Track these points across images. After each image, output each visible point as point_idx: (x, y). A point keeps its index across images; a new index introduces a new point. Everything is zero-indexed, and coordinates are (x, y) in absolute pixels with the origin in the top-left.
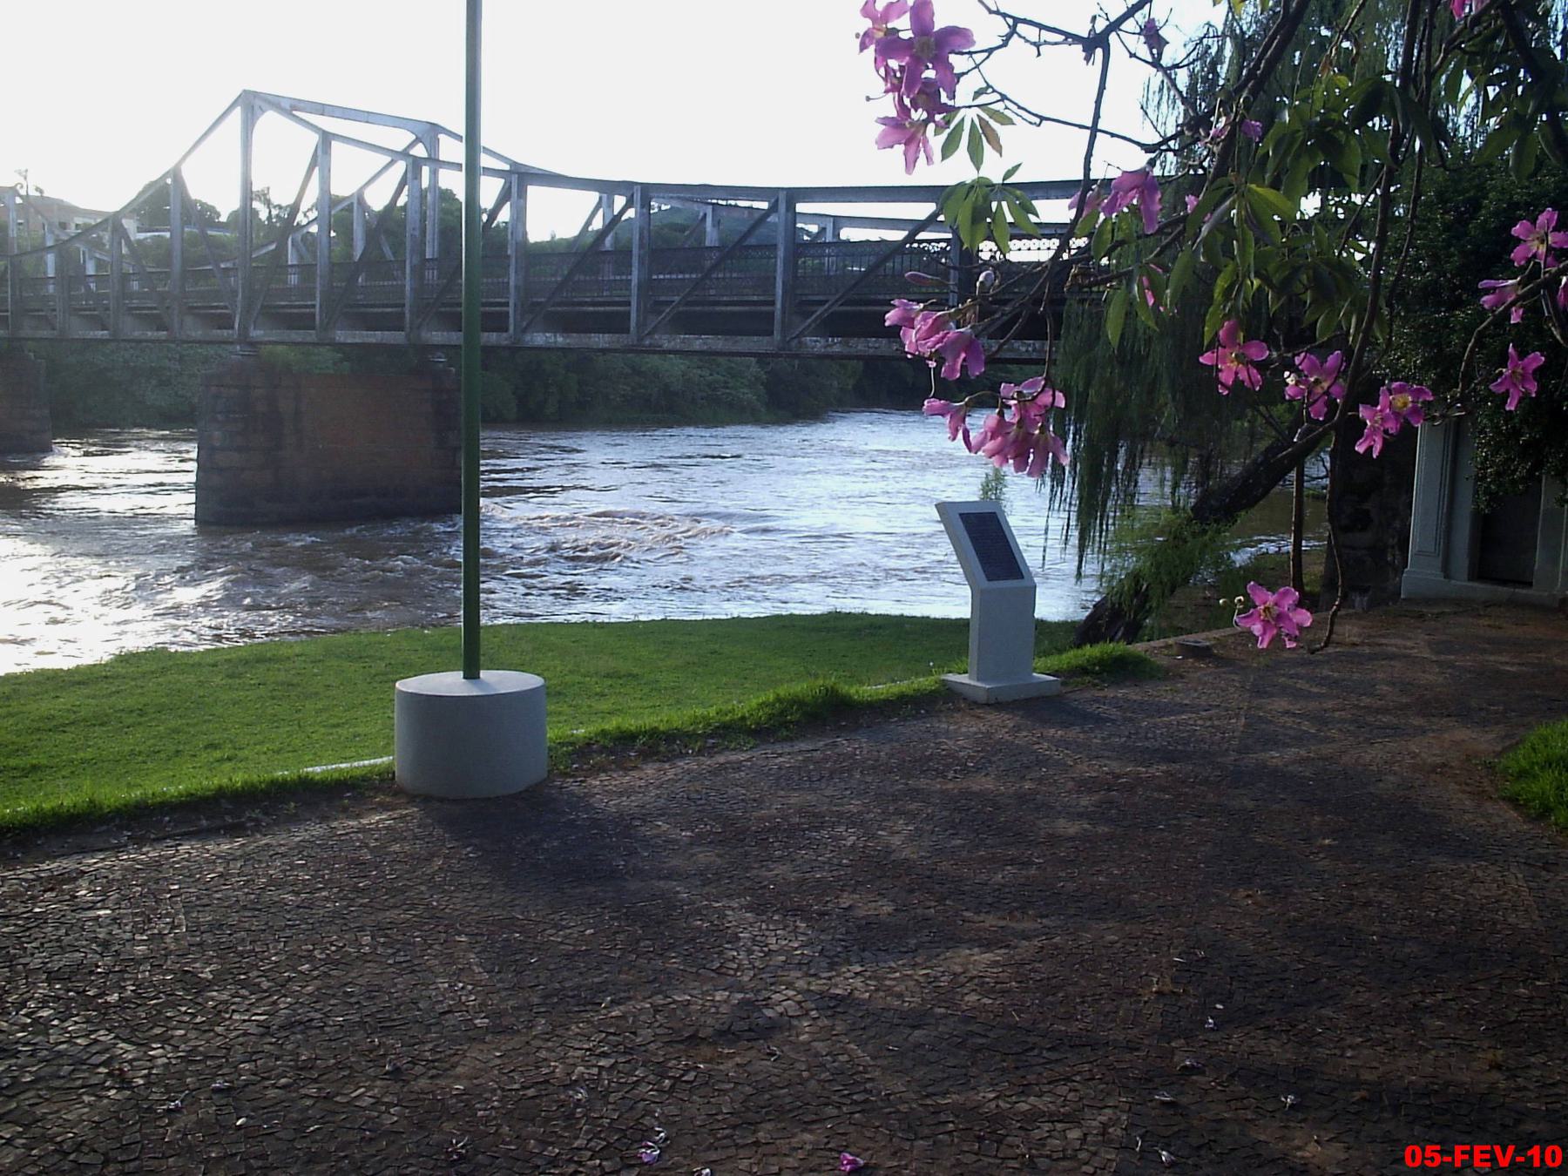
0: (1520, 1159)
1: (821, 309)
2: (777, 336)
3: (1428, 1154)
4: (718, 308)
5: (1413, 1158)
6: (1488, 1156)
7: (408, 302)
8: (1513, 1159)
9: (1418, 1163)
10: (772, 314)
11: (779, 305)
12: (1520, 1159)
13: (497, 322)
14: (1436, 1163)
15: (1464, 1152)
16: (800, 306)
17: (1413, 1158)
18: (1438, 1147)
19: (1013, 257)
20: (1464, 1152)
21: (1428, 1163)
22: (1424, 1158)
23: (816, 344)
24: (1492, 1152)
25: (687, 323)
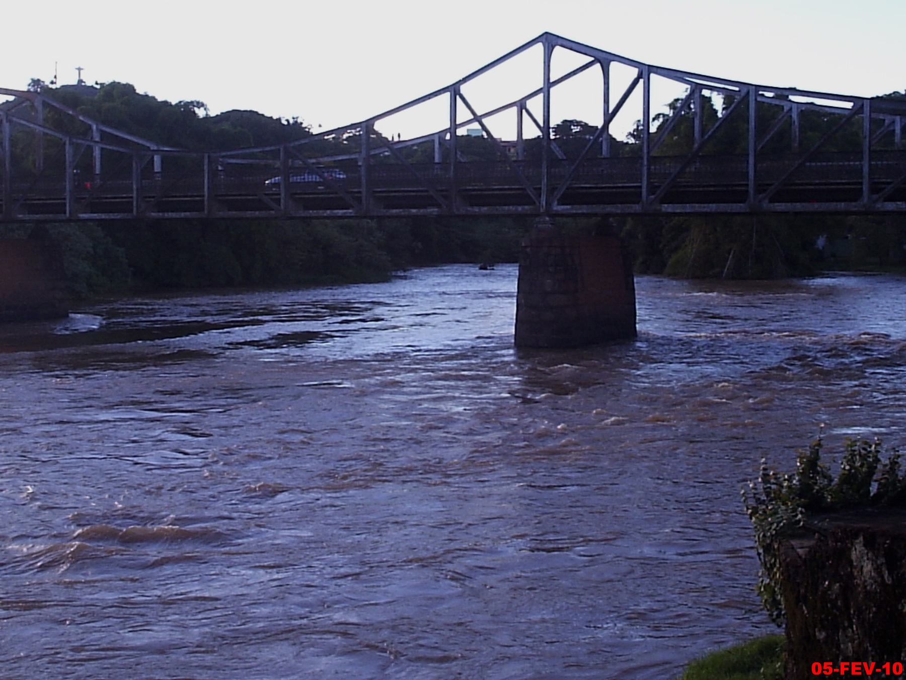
0: (878, 670)
1: (890, 187)
2: (206, 212)
3: (825, 668)
4: (793, 187)
5: (817, 670)
6: (859, 668)
7: (206, 194)
8: (874, 670)
9: (819, 673)
10: (747, 191)
11: (283, 195)
12: (878, 670)
13: (197, 206)
14: (830, 673)
15: (846, 666)
16: (652, 189)
17: (817, 670)
18: (831, 663)
19: (159, 170)
20: (846, 666)
21: (825, 672)
22: (823, 670)
23: (766, 205)
24: (862, 666)
25: (93, 207)
